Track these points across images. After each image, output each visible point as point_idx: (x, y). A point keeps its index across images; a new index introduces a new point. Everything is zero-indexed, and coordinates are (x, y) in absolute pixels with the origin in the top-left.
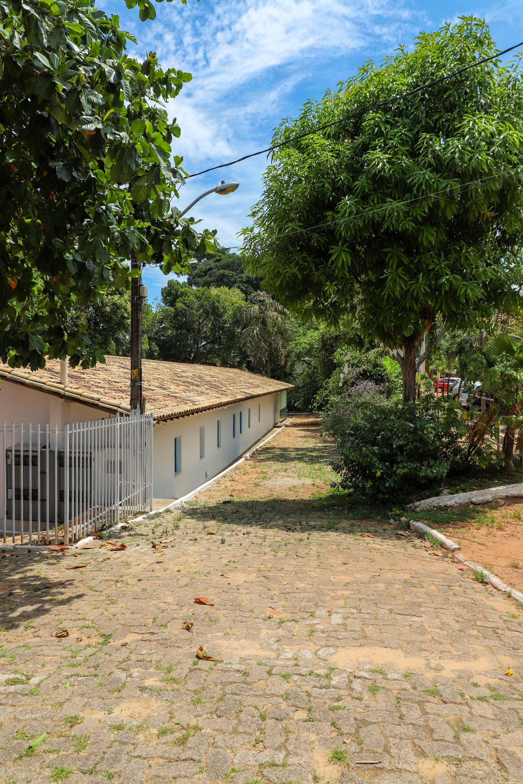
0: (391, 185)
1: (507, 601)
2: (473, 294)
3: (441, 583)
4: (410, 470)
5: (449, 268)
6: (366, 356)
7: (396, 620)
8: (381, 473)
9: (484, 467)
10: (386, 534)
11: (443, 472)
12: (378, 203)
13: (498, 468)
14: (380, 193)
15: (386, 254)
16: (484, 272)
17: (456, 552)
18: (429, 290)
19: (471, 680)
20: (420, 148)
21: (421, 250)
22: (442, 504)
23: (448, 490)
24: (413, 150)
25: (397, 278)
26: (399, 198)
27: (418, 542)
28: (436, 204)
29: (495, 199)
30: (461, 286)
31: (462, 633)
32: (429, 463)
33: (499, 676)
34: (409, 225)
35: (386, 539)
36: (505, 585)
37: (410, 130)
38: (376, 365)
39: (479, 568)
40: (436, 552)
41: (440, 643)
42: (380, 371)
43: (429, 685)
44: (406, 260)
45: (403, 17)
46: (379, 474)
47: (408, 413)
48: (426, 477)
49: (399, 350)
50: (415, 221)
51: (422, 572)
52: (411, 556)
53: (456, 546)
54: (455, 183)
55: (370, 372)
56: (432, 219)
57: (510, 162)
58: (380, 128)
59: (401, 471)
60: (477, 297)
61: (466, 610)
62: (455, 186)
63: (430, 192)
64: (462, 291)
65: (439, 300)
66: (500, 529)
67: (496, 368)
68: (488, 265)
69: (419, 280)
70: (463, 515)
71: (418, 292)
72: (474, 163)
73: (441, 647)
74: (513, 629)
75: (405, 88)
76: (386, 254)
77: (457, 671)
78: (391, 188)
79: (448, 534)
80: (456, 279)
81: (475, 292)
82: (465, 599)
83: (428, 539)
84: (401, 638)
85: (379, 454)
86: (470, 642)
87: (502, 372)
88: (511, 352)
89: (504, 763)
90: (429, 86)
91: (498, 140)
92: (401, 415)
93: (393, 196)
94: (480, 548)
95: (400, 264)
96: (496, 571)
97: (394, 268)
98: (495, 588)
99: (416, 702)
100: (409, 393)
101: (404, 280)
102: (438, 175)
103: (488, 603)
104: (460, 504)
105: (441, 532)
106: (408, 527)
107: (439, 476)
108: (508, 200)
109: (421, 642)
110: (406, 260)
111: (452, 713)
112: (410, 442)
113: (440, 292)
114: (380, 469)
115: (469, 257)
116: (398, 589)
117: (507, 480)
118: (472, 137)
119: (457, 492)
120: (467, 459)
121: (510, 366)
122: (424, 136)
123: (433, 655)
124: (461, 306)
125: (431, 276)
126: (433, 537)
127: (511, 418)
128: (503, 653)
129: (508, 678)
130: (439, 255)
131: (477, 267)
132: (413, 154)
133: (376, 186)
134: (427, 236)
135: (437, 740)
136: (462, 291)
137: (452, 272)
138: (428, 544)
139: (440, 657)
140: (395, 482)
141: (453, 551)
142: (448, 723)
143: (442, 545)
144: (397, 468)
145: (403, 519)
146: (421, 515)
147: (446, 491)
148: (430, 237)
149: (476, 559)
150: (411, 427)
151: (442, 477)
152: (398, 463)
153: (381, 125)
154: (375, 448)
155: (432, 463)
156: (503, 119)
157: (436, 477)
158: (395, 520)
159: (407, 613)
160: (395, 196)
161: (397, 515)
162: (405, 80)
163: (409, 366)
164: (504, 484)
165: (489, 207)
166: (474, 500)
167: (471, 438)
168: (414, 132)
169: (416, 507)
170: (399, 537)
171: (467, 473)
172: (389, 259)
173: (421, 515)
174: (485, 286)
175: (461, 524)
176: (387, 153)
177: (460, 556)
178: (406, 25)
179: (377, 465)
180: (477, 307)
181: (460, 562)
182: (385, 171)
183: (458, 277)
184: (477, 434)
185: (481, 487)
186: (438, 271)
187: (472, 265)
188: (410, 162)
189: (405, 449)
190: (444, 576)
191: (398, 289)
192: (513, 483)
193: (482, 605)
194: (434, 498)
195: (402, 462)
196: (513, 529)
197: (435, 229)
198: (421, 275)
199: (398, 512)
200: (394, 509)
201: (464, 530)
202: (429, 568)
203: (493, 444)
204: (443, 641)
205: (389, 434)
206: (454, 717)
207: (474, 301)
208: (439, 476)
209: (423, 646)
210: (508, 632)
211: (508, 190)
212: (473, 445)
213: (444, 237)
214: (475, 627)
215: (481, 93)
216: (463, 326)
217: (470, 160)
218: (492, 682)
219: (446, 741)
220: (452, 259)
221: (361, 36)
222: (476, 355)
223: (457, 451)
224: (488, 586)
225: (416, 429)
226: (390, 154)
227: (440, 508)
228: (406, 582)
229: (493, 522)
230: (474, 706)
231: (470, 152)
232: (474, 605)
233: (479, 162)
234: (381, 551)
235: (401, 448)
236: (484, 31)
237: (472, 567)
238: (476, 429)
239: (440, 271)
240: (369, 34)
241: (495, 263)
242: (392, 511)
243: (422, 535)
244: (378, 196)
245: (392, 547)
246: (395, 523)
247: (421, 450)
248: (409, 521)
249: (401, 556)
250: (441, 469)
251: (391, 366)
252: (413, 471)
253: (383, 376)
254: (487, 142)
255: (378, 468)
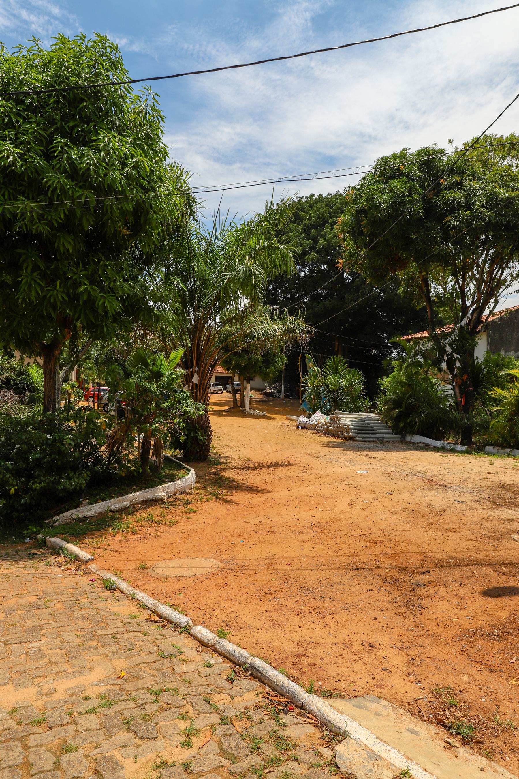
0: (23, 183)
1: (132, 604)
2: (111, 307)
3: (67, 599)
4: (48, 484)
5: (88, 279)
6: (9, 363)
7: (11, 651)
8: (15, 490)
9: (123, 475)
10: (17, 556)
11: (82, 484)
12: (10, 199)
13: (136, 474)
14: (12, 188)
15: (20, 255)
16: (122, 287)
17: (89, 563)
18: (67, 299)
19: (83, 695)
20: (55, 151)
21: (58, 257)
22: (81, 516)
23: (88, 501)
24: (48, 151)
25: (33, 283)
26: (33, 199)
27: (52, 559)
28: (72, 211)
29: (131, 220)
30: (99, 297)
31: (82, 648)
32: (68, 475)
33: (111, 682)
34: (43, 228)
35: (16, 561)
36: (130, 588)
37: (44, 130)
38: (21, 373)
39: (109, 576)
40: (69, 567)
41: (56, 664)
42: (25, 379)
43: (37, 714)
44: (42, 265)
45: (53, 13)
46: (13, 491)
47: (48, 425)
48: (64, 490)
49: (38, 359)
50: (50, 225)
51: (50, 590)
52: (43, 576)
53: (89, 557)
54: (90, 194)
55: (14, 380)
56: (68, 226)
57: (141, 186)
58: (10, 118)
59: (37, 486)
60: (115, 310)
61: (89, 622)
62: (91, 198)
63: (65, 198)
64: (101, 303)
65: (78, 309)
66: (134, 533)
67: (131, 380)
68: (125, 280)
69: (56, 287)
70: (101, 524)
71: (55, 300)
72: (109, 178)
73: (57, 669)
74: (132, 630)
75: (38, 84)
76: (20, 255)
77: (69, 689)
78: (24, 186)
79: (83, 545)
80: (93, 289)
81: (114, 306)
82: (90, 611)
83: (63, 554)
84: (13, 670)
85: (13, 469)
86: (87, 655)
87: (136, 384)
88: (146, 365)
89: (101, 771)
90: (64, 90)
91: (131, 162)
92: (39, 426)
93: (26, 195)
94: (112, 555)
95: (35, 268)
96: (124, 576)
97: (29, 271)
98: (122, 592)
99: (18, 739)
100: (49, 403)
101: (40, 285)
102: (74, 183)
103: (113, 609)
104: (100, 513)
105: (76, 545)
106: (43, 544)
107: (78, 488)
108: (142, 222)
109: (36, 669)
110: (42, 265)
111: (57, 738)
112: (48, 454)
113: (79, 301)
114: (14, 486)
115: (107, 270)
116: (20, 615)
117: (144, 486)
118: (107, 154)
119: (97, 502)
120: (107, 468)
121: (145, 378)
122: (58, 140)
123: (47, 679)
124: (100, 318)
125: (69, 284)
126: (68, 551)
127: (146, 427)
128: (118, 657)
129: (119, 682)
130: (78, 265)
131: (115, 281)
132: (48, 156)
133: (6, 180)
134: (63, 243)
135: (35, 774)
136: (101, 303)
137: (91, 283)
138: (62, 559)
139: (54, 680)
140: (32, 498)
141: (87, 562)
142: (50, 750)
143: (77, 558)
144: (33, 483)
145: (40, 536)
146: (58, 530)
147: (85, 502)
148: (67, 244)
149: (107, 567)
150: (49, 439)
151: (81, 488)
152: (34, 478)
153: (12, 116)
154: (9, 463)
155: (71, 475)
156: (134, 144)
157: (75, 489)
158: (31, 539)
159: (25, 640)
160: (28, 195)
161: (34, 533)
162: (40, 77)
163: (49, 374)
164: (141, 489)
165: (126, 225)
166: (113, 507)
167: (111, 448)
168: (48, 132)
169: (55, 522)
170: (32, 557)
171: (108, 481)
172: (24, 261)
173: (58, 530)
174: (123, 301)
175: (98, 533)
176: (19, 148)
177: (92, 567)
178: (57, 22)
179: (11, 481)
180: (115, 321)
181: (92, 572)
182: (16, 167)
183: (96, 288)
184: (116, 443)
185: (120, 494)
186: (75, 280)
187: (110, 278)
188: (44, 163)
189: (42, 462)
190: (74, 590)
191: (33, 293)
192: (149, 488)
193: (105, 613)
194: (74, 511)
195: (39, 476)
196: (146, 532)
197: (72, 237)
198: (58, 282)
199: (35, 530)
200: (30, 527)
201: (100, 539)
202: (57, 585)
203: (133, 453)
204: (60, 661)
205: (25, 447)
206: (58, 741)
207: (113, 314)
208: (78, 488)
209: (38, 673)
210: (126, 635)
211: (141, 213)
212: (112, 454)
213: (82, 247)
214: (96, 638)
215: (116, 114)
216: (104, 337)
217: (105, 175)
218: (103, 690)
219: (44, 772)
220: (90, 270)
221: (6, 13)
222: (113, 366)
223: (100, 460)
224: (115, 592)
225: (54, 440)
226: (22, 149)
227: (80, 520)
228: (30, 605)
229: (128, 527)
230: (81, 721)
231: (105, 168)
232: (98, 615)
233: (114, 180)
234: (8, 576)
235: (38, 462)
236: (117, 55)
237: (103, 575)
238: (115, 438)
239: (78, 280)
240: (14, 15)
241: (132, 279)
242: (27, 529)
243: (57, 551)
244: (9, 191)
245: (22, 569)
246: (31, 542)
247: (59, 463)
248: (45, 538)
249: (30, 578)
250: (80, 480)
251: (35, 373)
252: (51, 484)
253: (29, 385)
254: (120, 162)
255: (12, 484)
